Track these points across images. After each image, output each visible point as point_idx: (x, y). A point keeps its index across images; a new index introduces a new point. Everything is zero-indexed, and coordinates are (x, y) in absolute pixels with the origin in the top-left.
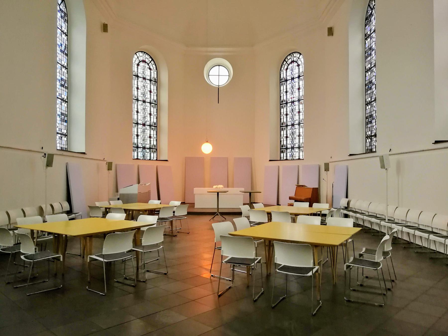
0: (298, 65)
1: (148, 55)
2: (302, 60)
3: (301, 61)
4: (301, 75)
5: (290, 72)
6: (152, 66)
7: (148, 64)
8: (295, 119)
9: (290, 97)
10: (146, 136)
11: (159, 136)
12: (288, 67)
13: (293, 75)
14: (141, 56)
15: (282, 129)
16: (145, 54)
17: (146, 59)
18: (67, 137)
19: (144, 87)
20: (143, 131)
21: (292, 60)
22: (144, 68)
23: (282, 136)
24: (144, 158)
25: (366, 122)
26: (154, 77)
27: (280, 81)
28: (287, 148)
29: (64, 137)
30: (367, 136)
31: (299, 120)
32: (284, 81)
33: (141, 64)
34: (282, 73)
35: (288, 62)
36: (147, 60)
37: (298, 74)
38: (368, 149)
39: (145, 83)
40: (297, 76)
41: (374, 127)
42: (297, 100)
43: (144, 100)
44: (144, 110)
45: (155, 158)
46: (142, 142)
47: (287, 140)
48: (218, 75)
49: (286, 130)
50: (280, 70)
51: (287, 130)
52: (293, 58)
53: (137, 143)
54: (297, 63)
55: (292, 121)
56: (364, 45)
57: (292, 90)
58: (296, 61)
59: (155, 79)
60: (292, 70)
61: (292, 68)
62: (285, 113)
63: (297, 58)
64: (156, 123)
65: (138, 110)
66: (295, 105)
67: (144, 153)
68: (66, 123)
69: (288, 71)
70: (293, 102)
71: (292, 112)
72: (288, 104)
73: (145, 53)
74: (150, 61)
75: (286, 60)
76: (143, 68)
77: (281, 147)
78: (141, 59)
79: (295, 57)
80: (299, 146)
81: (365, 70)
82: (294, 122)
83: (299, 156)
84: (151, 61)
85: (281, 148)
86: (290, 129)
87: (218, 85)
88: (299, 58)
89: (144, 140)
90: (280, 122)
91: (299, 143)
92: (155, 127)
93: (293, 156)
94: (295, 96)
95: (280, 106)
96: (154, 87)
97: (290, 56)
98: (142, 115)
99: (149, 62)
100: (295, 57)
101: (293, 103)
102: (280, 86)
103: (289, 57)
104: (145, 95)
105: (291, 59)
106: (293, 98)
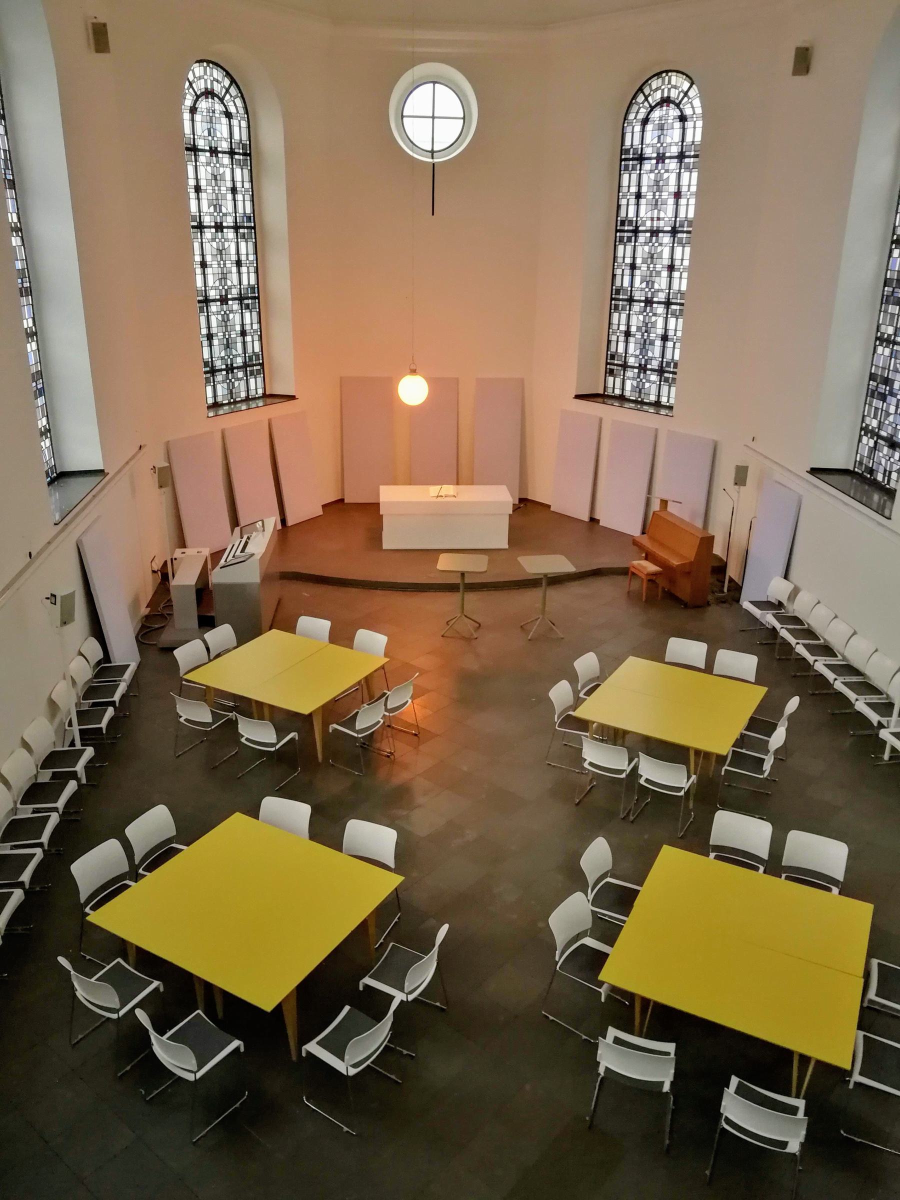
0: (683, 119)
1: (219, 68)
2: (697, 103)
3: (693, 107)
4: (687, 154)
5: (656, 133)
6: (232, 103)
7: (222, 100)
8: (656, 286)
9: (649, 215)
10: (232, 333)
11: (263, 256)
12: (649, 113)
13: (665, 145)
14: (200, 78)
15: (616, 307)
16: (211, 65)
17: (214, 82)
18: (37, 337)
19: (216, 179)
20: (223, 320)
21: (666, 95)
22: (211, 114)
23: (625, 190)
24: (232, 398)
26: (241, 140)
27: (621, 155)
28: (625, 366)
29: (15, 235)
30: (879, 334)
32: (633, 159)
33: (203, 104)
34: (629, 129)
35: (650, 99)
36: (217, 88)
37: (680, 147)
38: (861, 463)
39: (218, 165)
40: (677, 154)
41: (891, 418)
43: (219, 221)
44: (221, 254)
45: (260, 392)
46: (223, 354)
47: (638, 205)
48: (431, 115)
49: (627, 312)
50: (625, 119)
51: (629, 314)
52: (669, 90)
53: (198, 214)
55: (647, 290)
58: (677, 101)
59: (244, 146)
60: (661, 128)
61: (663, 122)
62: (628, 261)
63: (682, 95)
64: (251, 217)
65: (203, 258)
66: (661, 244)
67: (231, 383)
68: (13, 190)
69: (649, 127)
70: (655, 232)
72: (640, 234)
73: (209, 62)
74: (227, 86)
75: (647, 91)
76: (208, 117)
77: (614, 293)
78: (200, 86)
79: (675, 87)
82: (653, 293)
83: (659, 396)
84: (230, 87)
85: (618, 228)
86: (641, 313)
88: (686, 94)
89: (227, 346)
90: (612, 286)
91: (660, 359)
92: (253, 301)
94: (662, 215)
95: (610, 289)
97: (660, 80)
98: (216, 271)
99: (224, 91)
100: (675, 87)
102: (620, 171)
103: (655, 84)
104: (220, 206)
105: (663, 91)
106: (658, 219)
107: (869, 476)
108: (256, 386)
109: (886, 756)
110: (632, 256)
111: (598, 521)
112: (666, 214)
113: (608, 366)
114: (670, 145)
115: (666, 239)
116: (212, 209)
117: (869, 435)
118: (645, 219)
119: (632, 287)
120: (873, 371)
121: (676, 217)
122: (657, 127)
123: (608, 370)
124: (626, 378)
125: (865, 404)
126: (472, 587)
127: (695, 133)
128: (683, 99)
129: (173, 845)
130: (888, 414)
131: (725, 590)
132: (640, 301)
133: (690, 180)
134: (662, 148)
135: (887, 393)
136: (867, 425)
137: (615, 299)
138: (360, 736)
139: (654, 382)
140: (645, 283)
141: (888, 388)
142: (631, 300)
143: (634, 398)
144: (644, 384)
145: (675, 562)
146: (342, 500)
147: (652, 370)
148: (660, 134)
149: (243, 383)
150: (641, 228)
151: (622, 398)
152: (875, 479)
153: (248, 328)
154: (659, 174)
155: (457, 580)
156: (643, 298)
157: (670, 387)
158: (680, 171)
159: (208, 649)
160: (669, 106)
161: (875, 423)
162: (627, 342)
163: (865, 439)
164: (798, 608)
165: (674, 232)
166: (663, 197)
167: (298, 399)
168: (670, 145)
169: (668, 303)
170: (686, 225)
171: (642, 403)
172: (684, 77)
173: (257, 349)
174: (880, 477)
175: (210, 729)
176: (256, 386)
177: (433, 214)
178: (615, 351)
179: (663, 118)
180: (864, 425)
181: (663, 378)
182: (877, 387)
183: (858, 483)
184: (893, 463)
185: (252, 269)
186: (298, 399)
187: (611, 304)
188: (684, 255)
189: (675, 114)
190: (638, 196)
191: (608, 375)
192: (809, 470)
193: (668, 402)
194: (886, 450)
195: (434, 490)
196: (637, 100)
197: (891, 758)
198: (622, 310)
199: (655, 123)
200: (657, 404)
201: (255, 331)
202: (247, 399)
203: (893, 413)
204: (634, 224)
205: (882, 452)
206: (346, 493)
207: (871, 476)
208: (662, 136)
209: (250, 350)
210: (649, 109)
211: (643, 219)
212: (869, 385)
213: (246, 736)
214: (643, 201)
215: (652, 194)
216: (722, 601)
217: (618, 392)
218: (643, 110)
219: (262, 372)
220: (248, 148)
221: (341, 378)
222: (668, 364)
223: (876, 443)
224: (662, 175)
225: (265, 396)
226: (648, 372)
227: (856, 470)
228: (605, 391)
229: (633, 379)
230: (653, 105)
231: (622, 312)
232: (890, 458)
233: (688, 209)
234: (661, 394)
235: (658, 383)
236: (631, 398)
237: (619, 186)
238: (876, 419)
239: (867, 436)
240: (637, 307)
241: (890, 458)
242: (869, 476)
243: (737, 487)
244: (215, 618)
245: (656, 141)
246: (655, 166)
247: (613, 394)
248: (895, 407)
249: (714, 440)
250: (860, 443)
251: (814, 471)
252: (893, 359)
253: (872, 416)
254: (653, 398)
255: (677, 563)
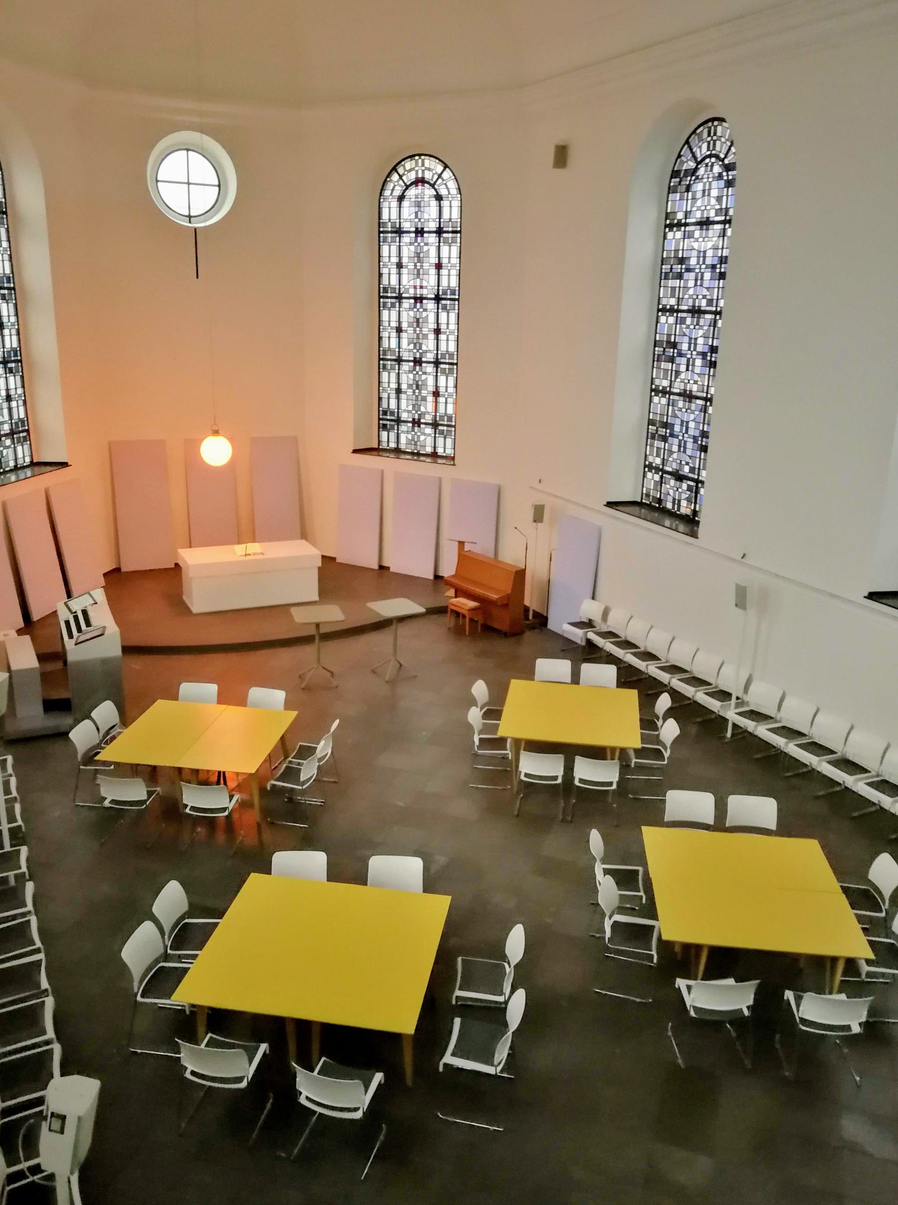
4: (445, 229)
5: (413, 210)
8: (424, 348)
9: (412, 283)
13: (422, 220)
25: (661, 273)
27: (379, 227)
31: (437, 354)
34: (385, 205)
35: (404, 178)
38: (648, 495)
42: (433, 296)
45: (28, 460)
47: (399, 274)
49: (397, 371)
50: (381, 194)
51: (399, 373)
52: (423, 171)
54: (436, 190)
56: (655, 324)
57: (418, 264)
60: (418, 205)
61: (419, 200)
62: (394, 324)
63: (436, 177)
69: (405, 203)
70: (419, 299)
71: (415, 326)
75: (401, 170)
79: (429, 169)
80: (437, 358)
81: (651, 387)
83: (435, 447)
87: (187, 214)
88: (440, 176)
90: (379, 347)
93: (416, 444)
94: (425, 284)
96: (8, 305)
97: (413, 162)
100: (429, 169)
101: (419, 301)
103: (408, 164)
105: (417, 172)
106: (421, 287)
107: (657, 505)
108: (23, 453)
109: (729, 734)
110: (397, 320)
111: (388, 568)
112: (428, 283)
113: (381, 422)
114: (428, 220)
115: (431, 305)
117: (653, 471)
118: (408, 287)
119: (399, 348)
120: (651, 418)
121: (438, 286)
122: (413, 204)
123: (381, 425)
124: (400, 432)
125: (647, 445)
126: (327, 637)
127: (452, 211)
128: (437, 180)
129: (186, 921)
130: (671, 452)
131: (531, 617)
132: (409, 361)
133: (451, 253)
134: (420, 223)
135: (668, 435)
136: (651, 464)
137: (383, 359)
138: (304, 787)
139: (429, 435)
140: (413, 345)
141: (668, 431)
142: (399, 360)
143: (410, 451)
144: (419, 436)
145: (494, 596)
146: (117, 570)
147: (426, 424)
148: (417, 210)
149: (11, 451)
150: (404, 295)
151: (397, 451)
152: (665, 508)
153: (12, 392)
154: (419, 247)
155: (312, 631)
156: (412, 359)
157: (445, 438)
158: (439, 245)
159: (98, 729)
160: (424, 186)
161: (658, 461)
162: (398, 399)
163: (649, 475)
164: (615, 623)
165: (438, 299)
166: (424, 268)
167: (71, 465)
168: (428, 220)
169: (437, 363)
170: (449, 293)
171: (418, 454)
172: (437, 161)
173: (22, 415)
174: (669, 506)
175: (145, 806)
176: (23, 453)
177: (197, 278)
178: (387, 407)
179: (419, 197)
180: (647, 463)
181: (437, 430)
182: (657, 431)
183: (647, 512)
184: (681, 493)
185: (14, 332)
186: (71, 465)
187: (379, 364)
188: (448, 320)
189: (431, 193)
190: (400, 266)
191: (381, 430)
192: (605, 504)
193: (444, 452)
194: (672, 482)
195: (239, 550)
196: (392, 178)
197: (733, 735)
198: (391, 369)
199: (412, 200)
200: (434, 455)
201: (20, 396)
202: (16, 468)
203: (677, 450)
204: (397, 292)
205: (669, 485)
206: (122, 564)
207: (659, 506)
208: (419, 213)
209: (15, 416)
210: (405, 187)
211: (406, 287)
212: (648, 429)
213: (190, 805)
214: (404, 271)
215: (413, 264)
216: (532, 628)
217: (393, 445)
219: (28, 439)
220: (4, 206)
221: (110, 445)
222: (442, 417)
223: (662, 477)
224: (422, 248)
225: (33, 464)
226: (422, 426)
227: (644, 501)
228: (379, 445)
230: (408, 184)
231: (391, 371)
232: (678, 489)
233: (450, 280)
234: (437, 446)
235: (433, 435)
236: (407, 450)
237: (380, 256)
238: (660, 457)
239: (651, 472)
240: (406, 367)
241: (678, 489)
242: (657, 505)
243: (535, 524)
244: (72, 701)
245: (413, 216)
246: (414, 239)
247: (388, 448)
248: (687, 447)
249: (498, 485)
250: (645, 479)
251: (610, 504)
252: (670, 408)
253: (655, 455)
254: (429, 450)
255: (497, 597)
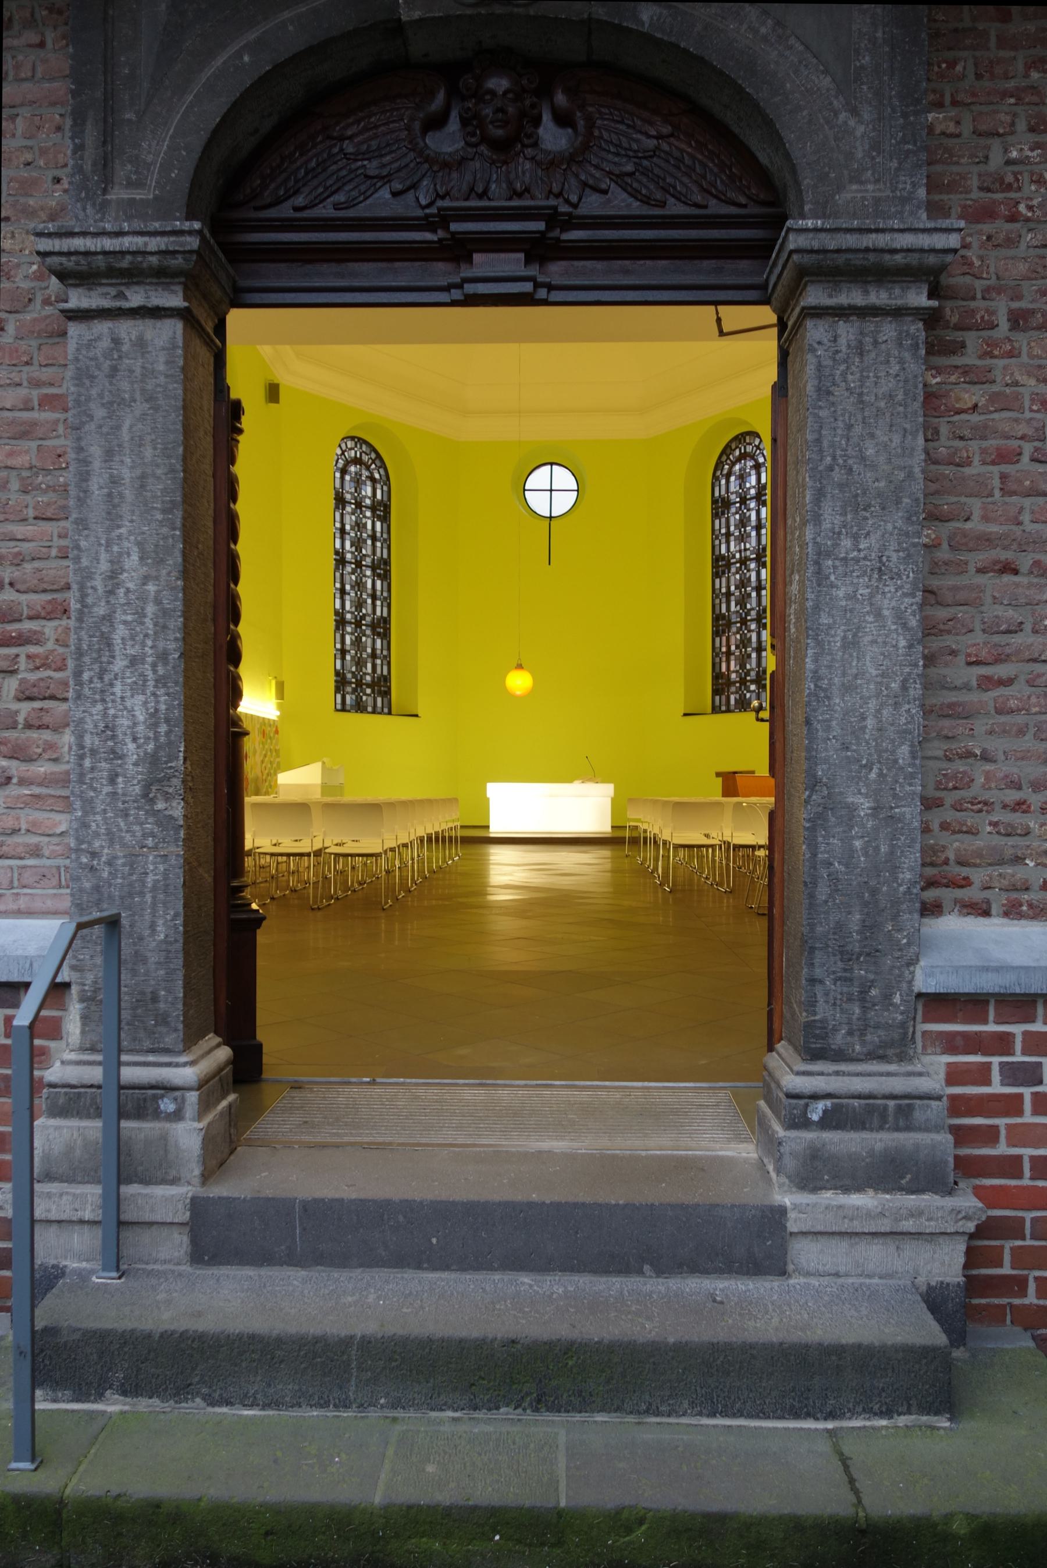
5: (738, 482)
36: (365, 458)
69: (733, 478)
94: (748, 546)
100: (750, 444)
114: (749, 489)
116: (353, 549)
168: (749, 489)
218: (727, 467)
229: (736, 693)
